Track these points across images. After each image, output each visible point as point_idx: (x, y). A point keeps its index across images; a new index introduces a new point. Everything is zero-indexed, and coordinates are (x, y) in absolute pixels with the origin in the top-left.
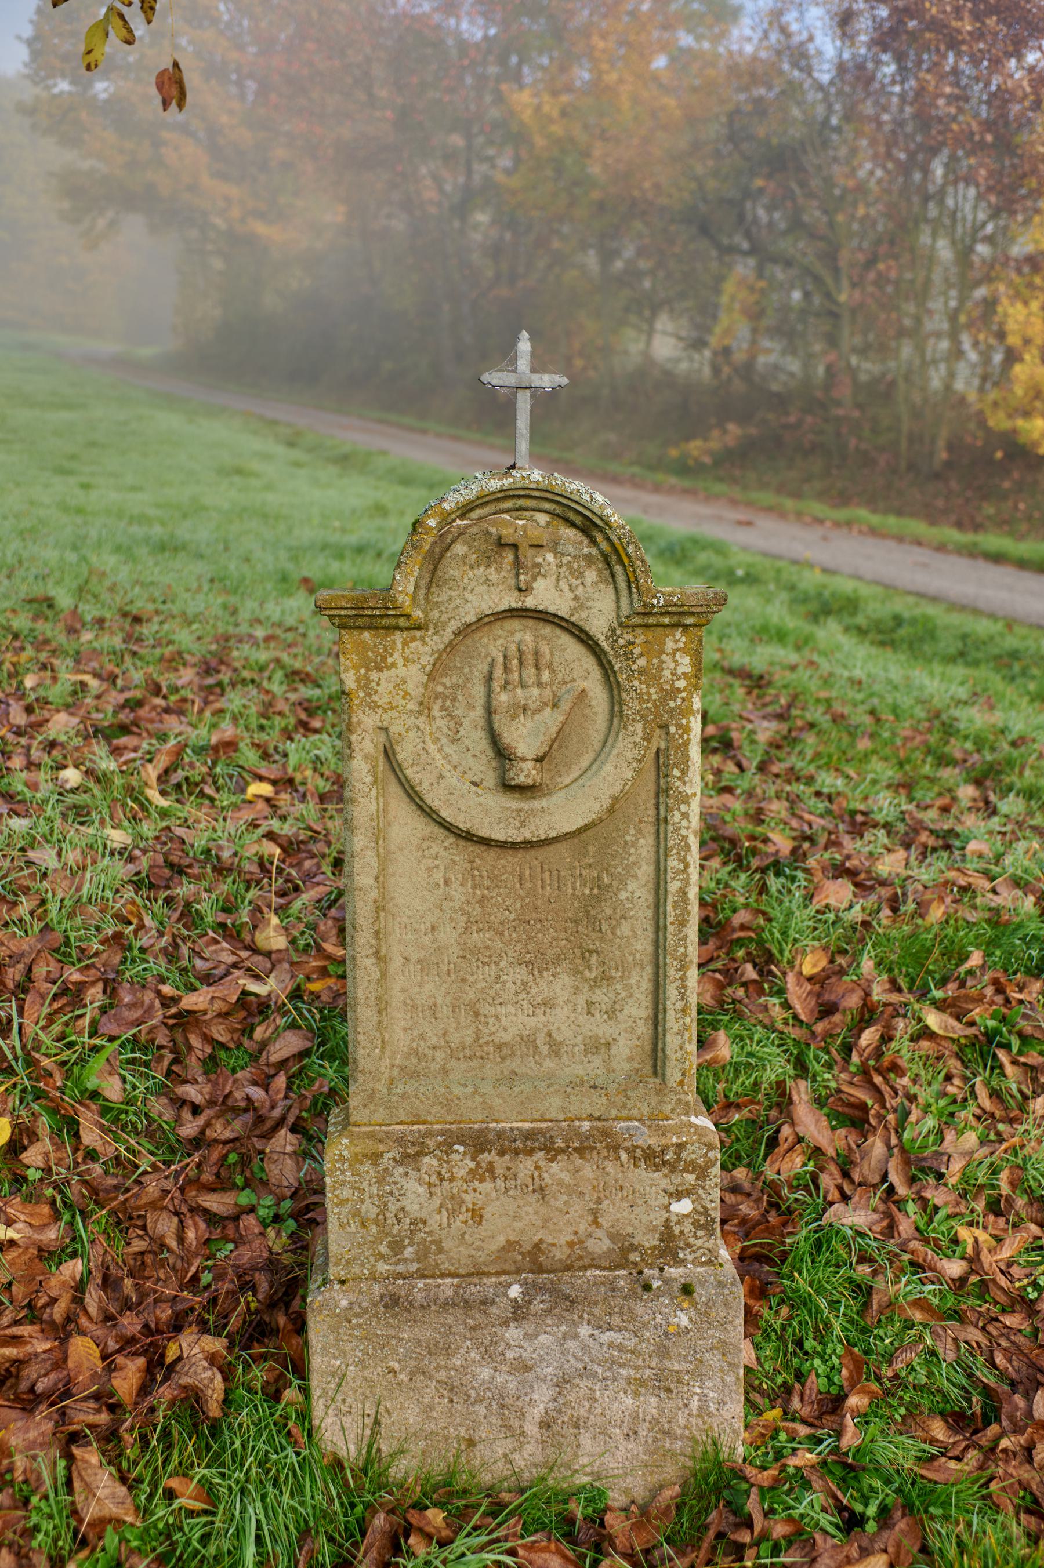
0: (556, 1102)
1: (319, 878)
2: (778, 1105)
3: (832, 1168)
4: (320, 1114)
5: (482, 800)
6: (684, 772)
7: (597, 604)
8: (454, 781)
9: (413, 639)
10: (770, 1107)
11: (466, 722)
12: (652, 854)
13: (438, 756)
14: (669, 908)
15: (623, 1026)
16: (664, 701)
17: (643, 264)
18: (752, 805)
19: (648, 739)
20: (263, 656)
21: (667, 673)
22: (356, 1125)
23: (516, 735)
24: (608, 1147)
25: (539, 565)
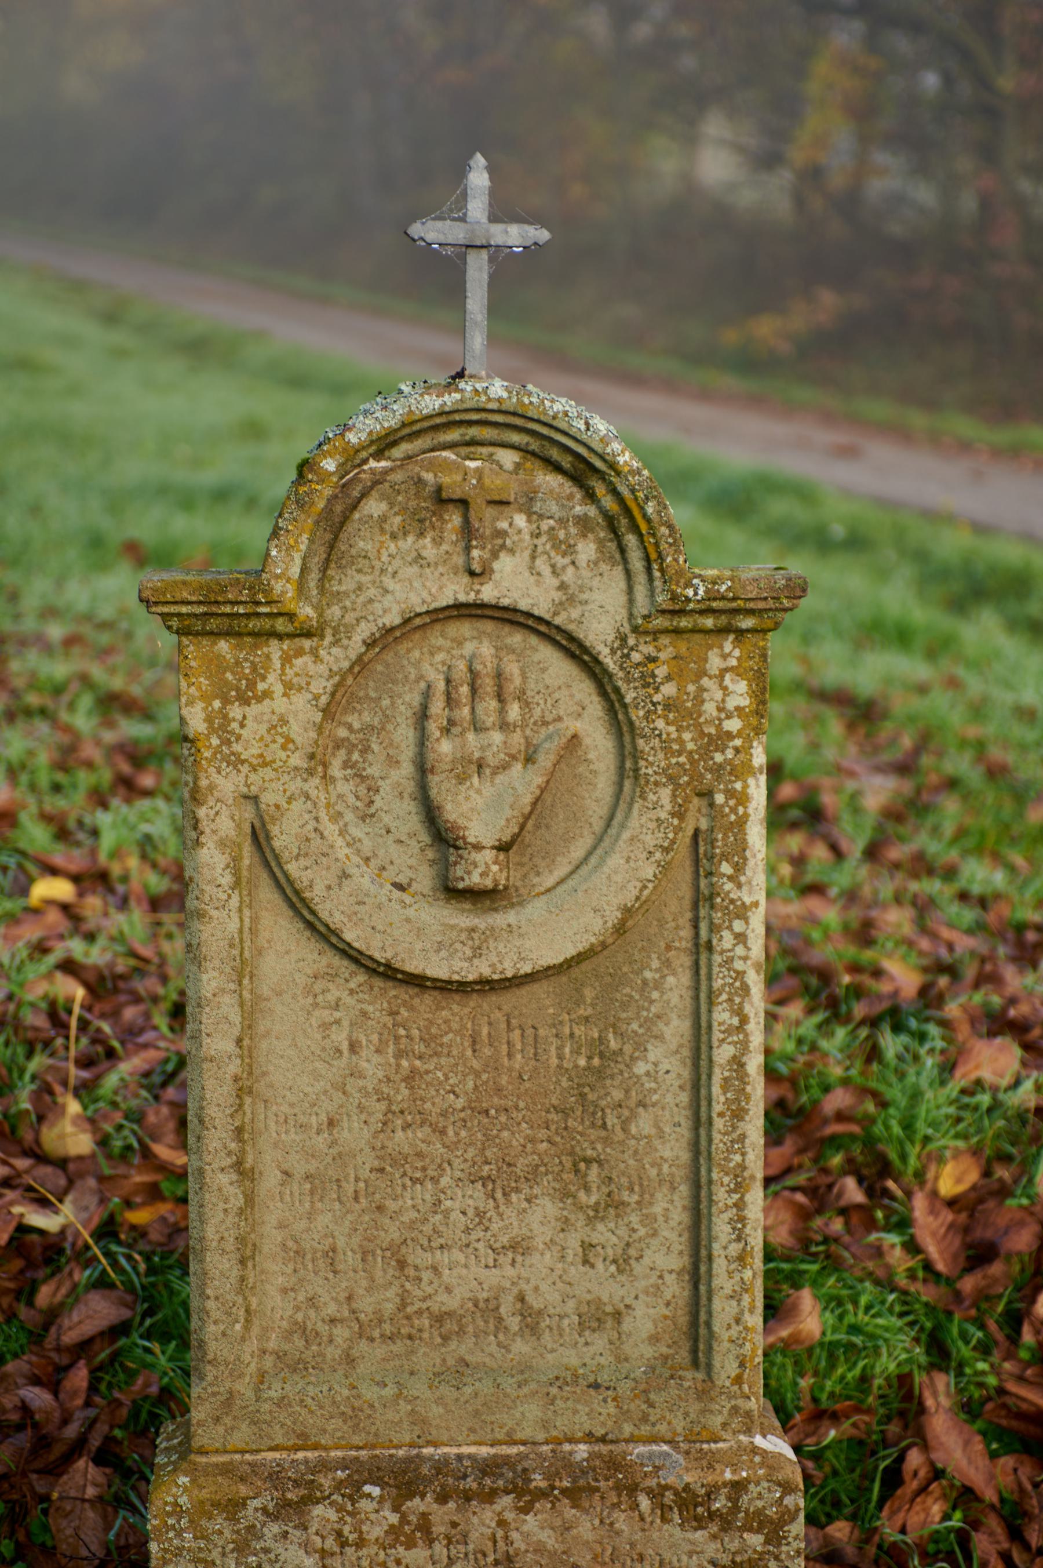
0: (533, 1411)
1: (148, 1036)
2: (902, 1414)
3: (993, 1522)
4: (144, 1432)
5: (411, 912)
6: (739, 868)
7: (597, 597)
8: (366, 882)
9: (300, 653)
10: (888, 1419)
11: (385, 786)
12: (688, 1001)
13: (340, 842)
14: (716, 1090)
15: (642, 1284)
16: (706, 752)
17: (683, 30)
18: (855, 915)
19: (679, 814)
20: (59, 669)
21: (710, 708)
22: (203, 1452)
23: (465, 807)
24: (618, 1488)
25: (502, 534)
